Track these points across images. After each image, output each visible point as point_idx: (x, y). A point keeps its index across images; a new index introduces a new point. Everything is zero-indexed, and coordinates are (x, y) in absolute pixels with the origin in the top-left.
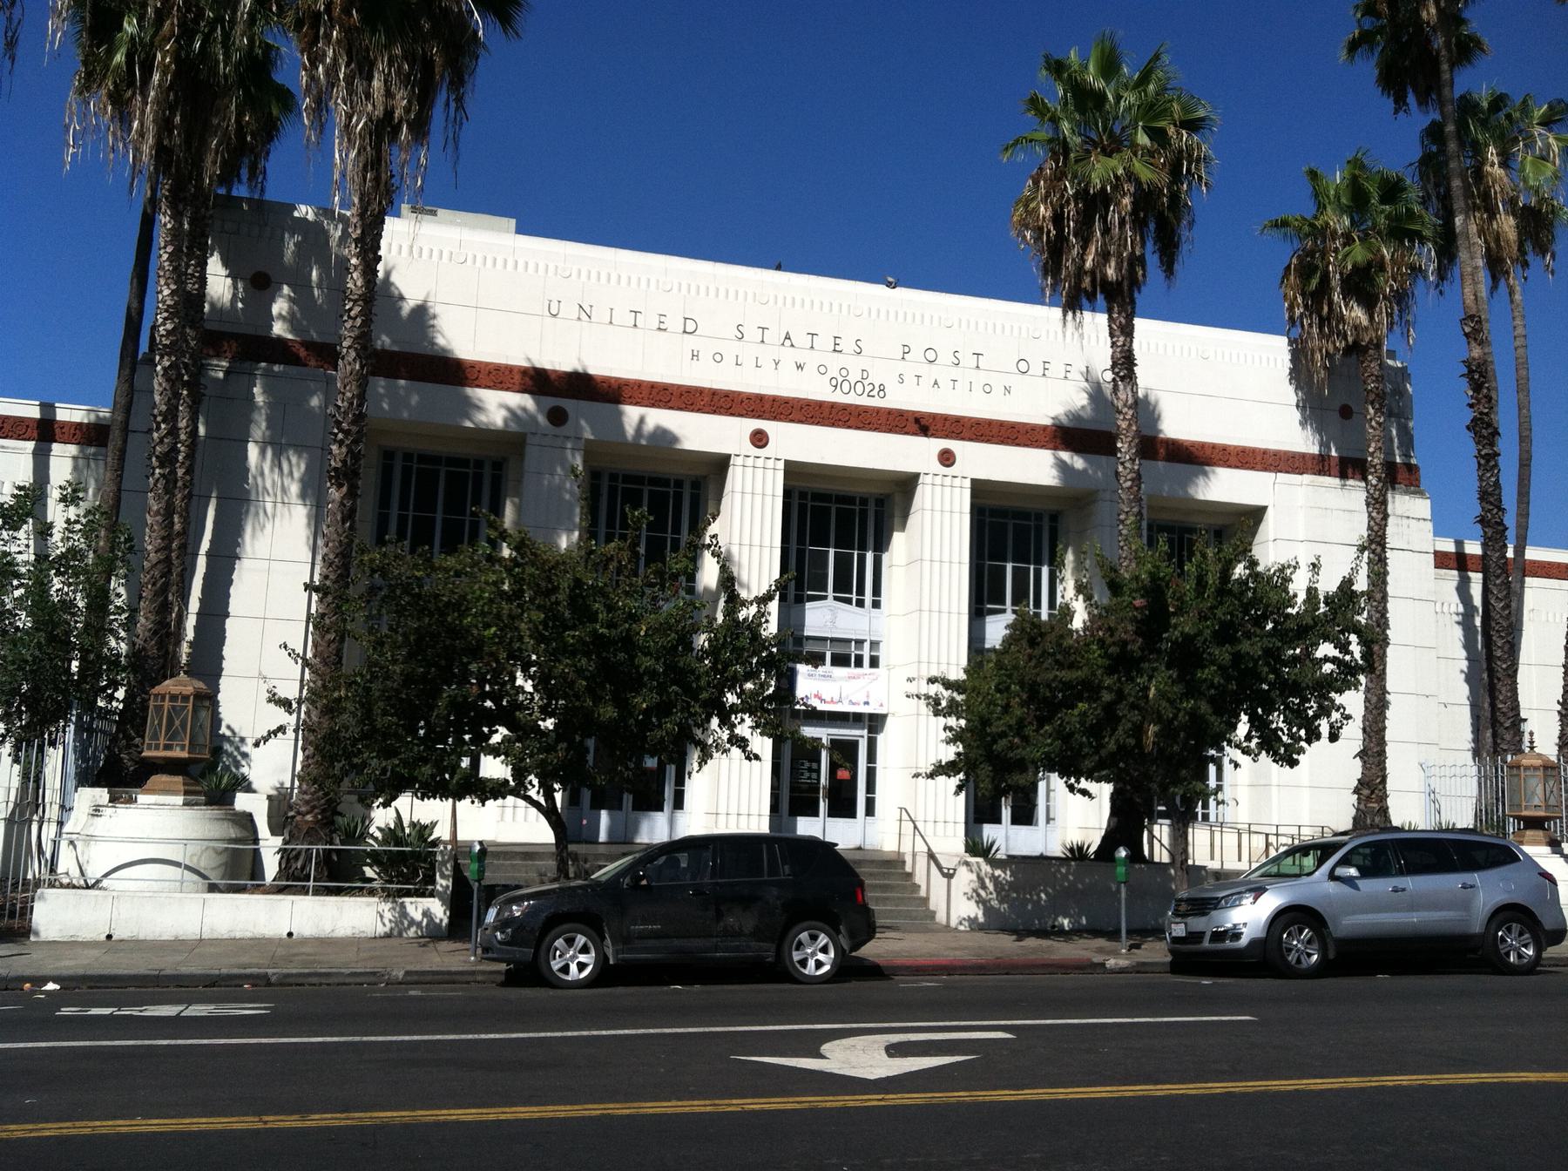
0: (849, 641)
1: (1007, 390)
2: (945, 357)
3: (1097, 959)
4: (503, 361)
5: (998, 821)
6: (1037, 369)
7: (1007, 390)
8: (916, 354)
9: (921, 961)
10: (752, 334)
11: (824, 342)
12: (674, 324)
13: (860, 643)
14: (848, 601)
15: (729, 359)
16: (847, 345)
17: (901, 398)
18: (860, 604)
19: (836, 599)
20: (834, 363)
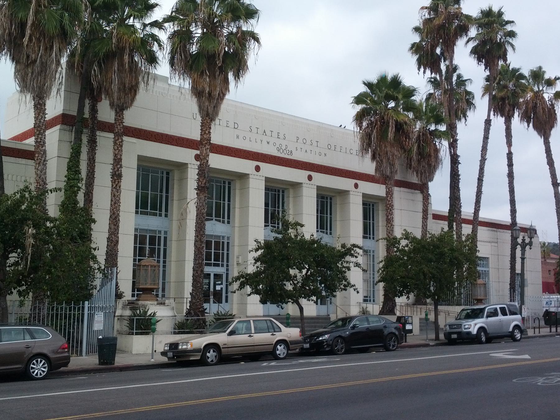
0: (220, 237)
1: (325, 155)
2: (309, 142)
3: (427, 343)
4: (140, 127)
5: (209, 302)
6: (333, 148)
7: (325, 155)
8: (300, 141)
9: (85, 367)
10: (254, 130)
11: (275, 134)
12: (231, 124)
13: (223, 237)
14: (219, 221)
15: (248, 139)
16: (281, 136)
17: (298, 156)
18: (370, 238)
19: (216, 220)
20: (278, 142)
